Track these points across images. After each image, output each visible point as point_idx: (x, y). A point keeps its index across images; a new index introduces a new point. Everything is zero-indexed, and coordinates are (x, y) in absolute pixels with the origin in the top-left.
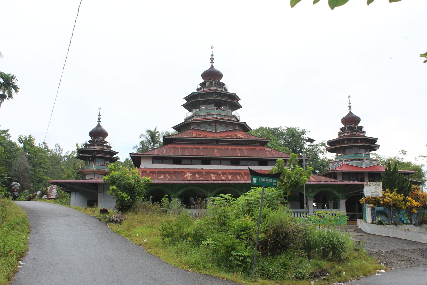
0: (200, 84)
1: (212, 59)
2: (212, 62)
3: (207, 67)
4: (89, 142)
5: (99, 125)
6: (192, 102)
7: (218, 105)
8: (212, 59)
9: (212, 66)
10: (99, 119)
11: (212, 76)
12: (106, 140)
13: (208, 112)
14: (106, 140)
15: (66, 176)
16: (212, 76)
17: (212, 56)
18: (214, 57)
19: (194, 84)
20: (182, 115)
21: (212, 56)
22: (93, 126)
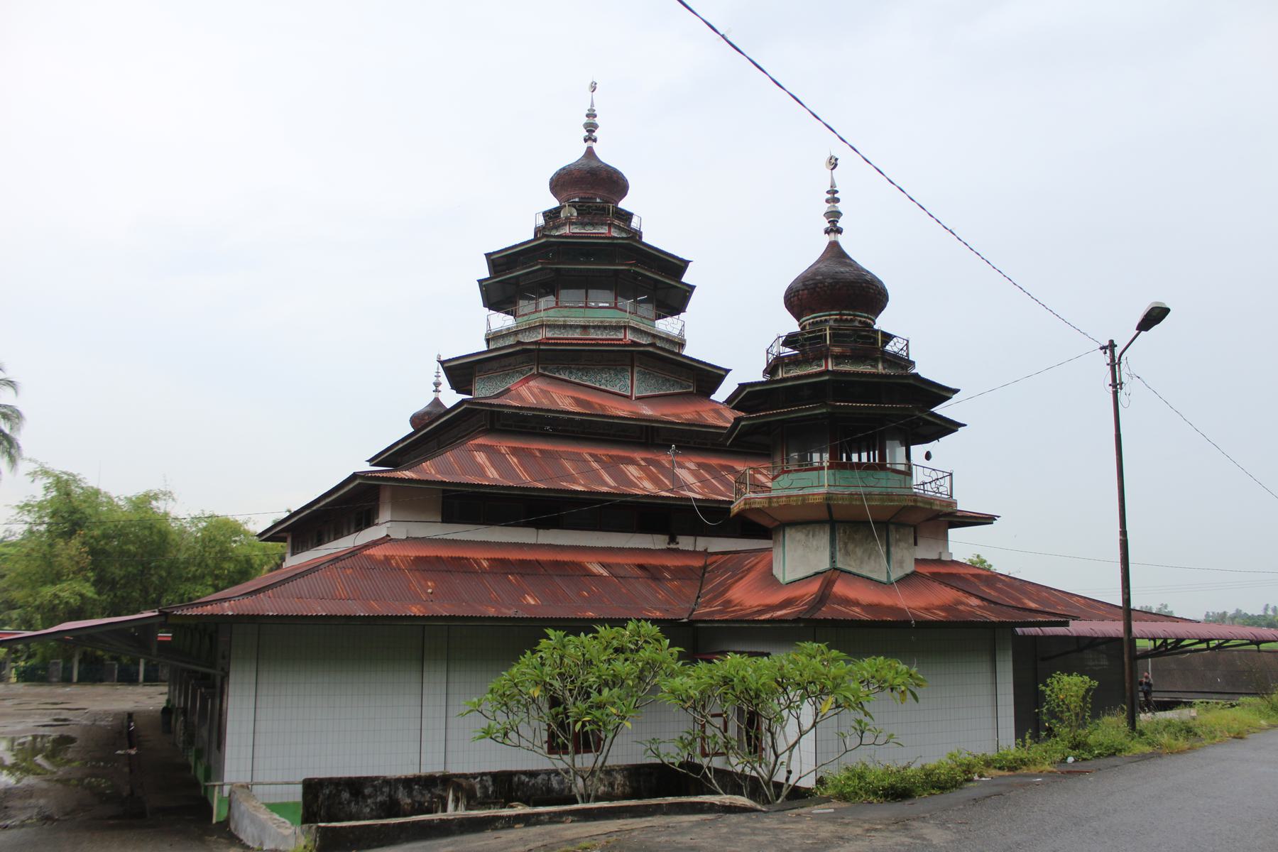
0: (545, 214)
1: (591, 128)
2: (590, 138)
3: (572, 154)
4: (790, 341)
5: (835, 252)
6: (509, 279)
7: (623, 286)
8: (591, 128)
9: (590, 152)
10: (834, 216)
11: (591, 187)
12: (883, 323)
13: (597, 314)
14: (883, 323)
15: (34, 646)
16: (591, 187)
17: (591, 115)
18: (597, 120)
19: (520, 216)
20: (473, 328)
21: (591, 115)
22: (802, 254)
